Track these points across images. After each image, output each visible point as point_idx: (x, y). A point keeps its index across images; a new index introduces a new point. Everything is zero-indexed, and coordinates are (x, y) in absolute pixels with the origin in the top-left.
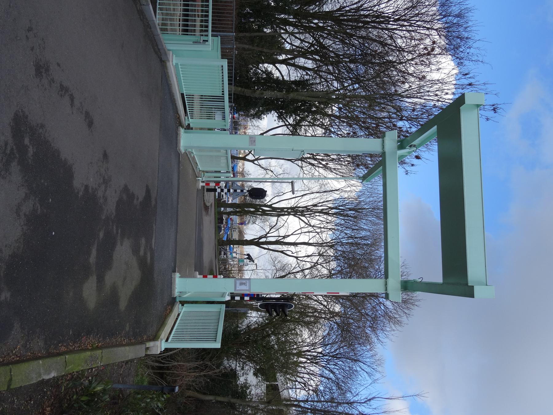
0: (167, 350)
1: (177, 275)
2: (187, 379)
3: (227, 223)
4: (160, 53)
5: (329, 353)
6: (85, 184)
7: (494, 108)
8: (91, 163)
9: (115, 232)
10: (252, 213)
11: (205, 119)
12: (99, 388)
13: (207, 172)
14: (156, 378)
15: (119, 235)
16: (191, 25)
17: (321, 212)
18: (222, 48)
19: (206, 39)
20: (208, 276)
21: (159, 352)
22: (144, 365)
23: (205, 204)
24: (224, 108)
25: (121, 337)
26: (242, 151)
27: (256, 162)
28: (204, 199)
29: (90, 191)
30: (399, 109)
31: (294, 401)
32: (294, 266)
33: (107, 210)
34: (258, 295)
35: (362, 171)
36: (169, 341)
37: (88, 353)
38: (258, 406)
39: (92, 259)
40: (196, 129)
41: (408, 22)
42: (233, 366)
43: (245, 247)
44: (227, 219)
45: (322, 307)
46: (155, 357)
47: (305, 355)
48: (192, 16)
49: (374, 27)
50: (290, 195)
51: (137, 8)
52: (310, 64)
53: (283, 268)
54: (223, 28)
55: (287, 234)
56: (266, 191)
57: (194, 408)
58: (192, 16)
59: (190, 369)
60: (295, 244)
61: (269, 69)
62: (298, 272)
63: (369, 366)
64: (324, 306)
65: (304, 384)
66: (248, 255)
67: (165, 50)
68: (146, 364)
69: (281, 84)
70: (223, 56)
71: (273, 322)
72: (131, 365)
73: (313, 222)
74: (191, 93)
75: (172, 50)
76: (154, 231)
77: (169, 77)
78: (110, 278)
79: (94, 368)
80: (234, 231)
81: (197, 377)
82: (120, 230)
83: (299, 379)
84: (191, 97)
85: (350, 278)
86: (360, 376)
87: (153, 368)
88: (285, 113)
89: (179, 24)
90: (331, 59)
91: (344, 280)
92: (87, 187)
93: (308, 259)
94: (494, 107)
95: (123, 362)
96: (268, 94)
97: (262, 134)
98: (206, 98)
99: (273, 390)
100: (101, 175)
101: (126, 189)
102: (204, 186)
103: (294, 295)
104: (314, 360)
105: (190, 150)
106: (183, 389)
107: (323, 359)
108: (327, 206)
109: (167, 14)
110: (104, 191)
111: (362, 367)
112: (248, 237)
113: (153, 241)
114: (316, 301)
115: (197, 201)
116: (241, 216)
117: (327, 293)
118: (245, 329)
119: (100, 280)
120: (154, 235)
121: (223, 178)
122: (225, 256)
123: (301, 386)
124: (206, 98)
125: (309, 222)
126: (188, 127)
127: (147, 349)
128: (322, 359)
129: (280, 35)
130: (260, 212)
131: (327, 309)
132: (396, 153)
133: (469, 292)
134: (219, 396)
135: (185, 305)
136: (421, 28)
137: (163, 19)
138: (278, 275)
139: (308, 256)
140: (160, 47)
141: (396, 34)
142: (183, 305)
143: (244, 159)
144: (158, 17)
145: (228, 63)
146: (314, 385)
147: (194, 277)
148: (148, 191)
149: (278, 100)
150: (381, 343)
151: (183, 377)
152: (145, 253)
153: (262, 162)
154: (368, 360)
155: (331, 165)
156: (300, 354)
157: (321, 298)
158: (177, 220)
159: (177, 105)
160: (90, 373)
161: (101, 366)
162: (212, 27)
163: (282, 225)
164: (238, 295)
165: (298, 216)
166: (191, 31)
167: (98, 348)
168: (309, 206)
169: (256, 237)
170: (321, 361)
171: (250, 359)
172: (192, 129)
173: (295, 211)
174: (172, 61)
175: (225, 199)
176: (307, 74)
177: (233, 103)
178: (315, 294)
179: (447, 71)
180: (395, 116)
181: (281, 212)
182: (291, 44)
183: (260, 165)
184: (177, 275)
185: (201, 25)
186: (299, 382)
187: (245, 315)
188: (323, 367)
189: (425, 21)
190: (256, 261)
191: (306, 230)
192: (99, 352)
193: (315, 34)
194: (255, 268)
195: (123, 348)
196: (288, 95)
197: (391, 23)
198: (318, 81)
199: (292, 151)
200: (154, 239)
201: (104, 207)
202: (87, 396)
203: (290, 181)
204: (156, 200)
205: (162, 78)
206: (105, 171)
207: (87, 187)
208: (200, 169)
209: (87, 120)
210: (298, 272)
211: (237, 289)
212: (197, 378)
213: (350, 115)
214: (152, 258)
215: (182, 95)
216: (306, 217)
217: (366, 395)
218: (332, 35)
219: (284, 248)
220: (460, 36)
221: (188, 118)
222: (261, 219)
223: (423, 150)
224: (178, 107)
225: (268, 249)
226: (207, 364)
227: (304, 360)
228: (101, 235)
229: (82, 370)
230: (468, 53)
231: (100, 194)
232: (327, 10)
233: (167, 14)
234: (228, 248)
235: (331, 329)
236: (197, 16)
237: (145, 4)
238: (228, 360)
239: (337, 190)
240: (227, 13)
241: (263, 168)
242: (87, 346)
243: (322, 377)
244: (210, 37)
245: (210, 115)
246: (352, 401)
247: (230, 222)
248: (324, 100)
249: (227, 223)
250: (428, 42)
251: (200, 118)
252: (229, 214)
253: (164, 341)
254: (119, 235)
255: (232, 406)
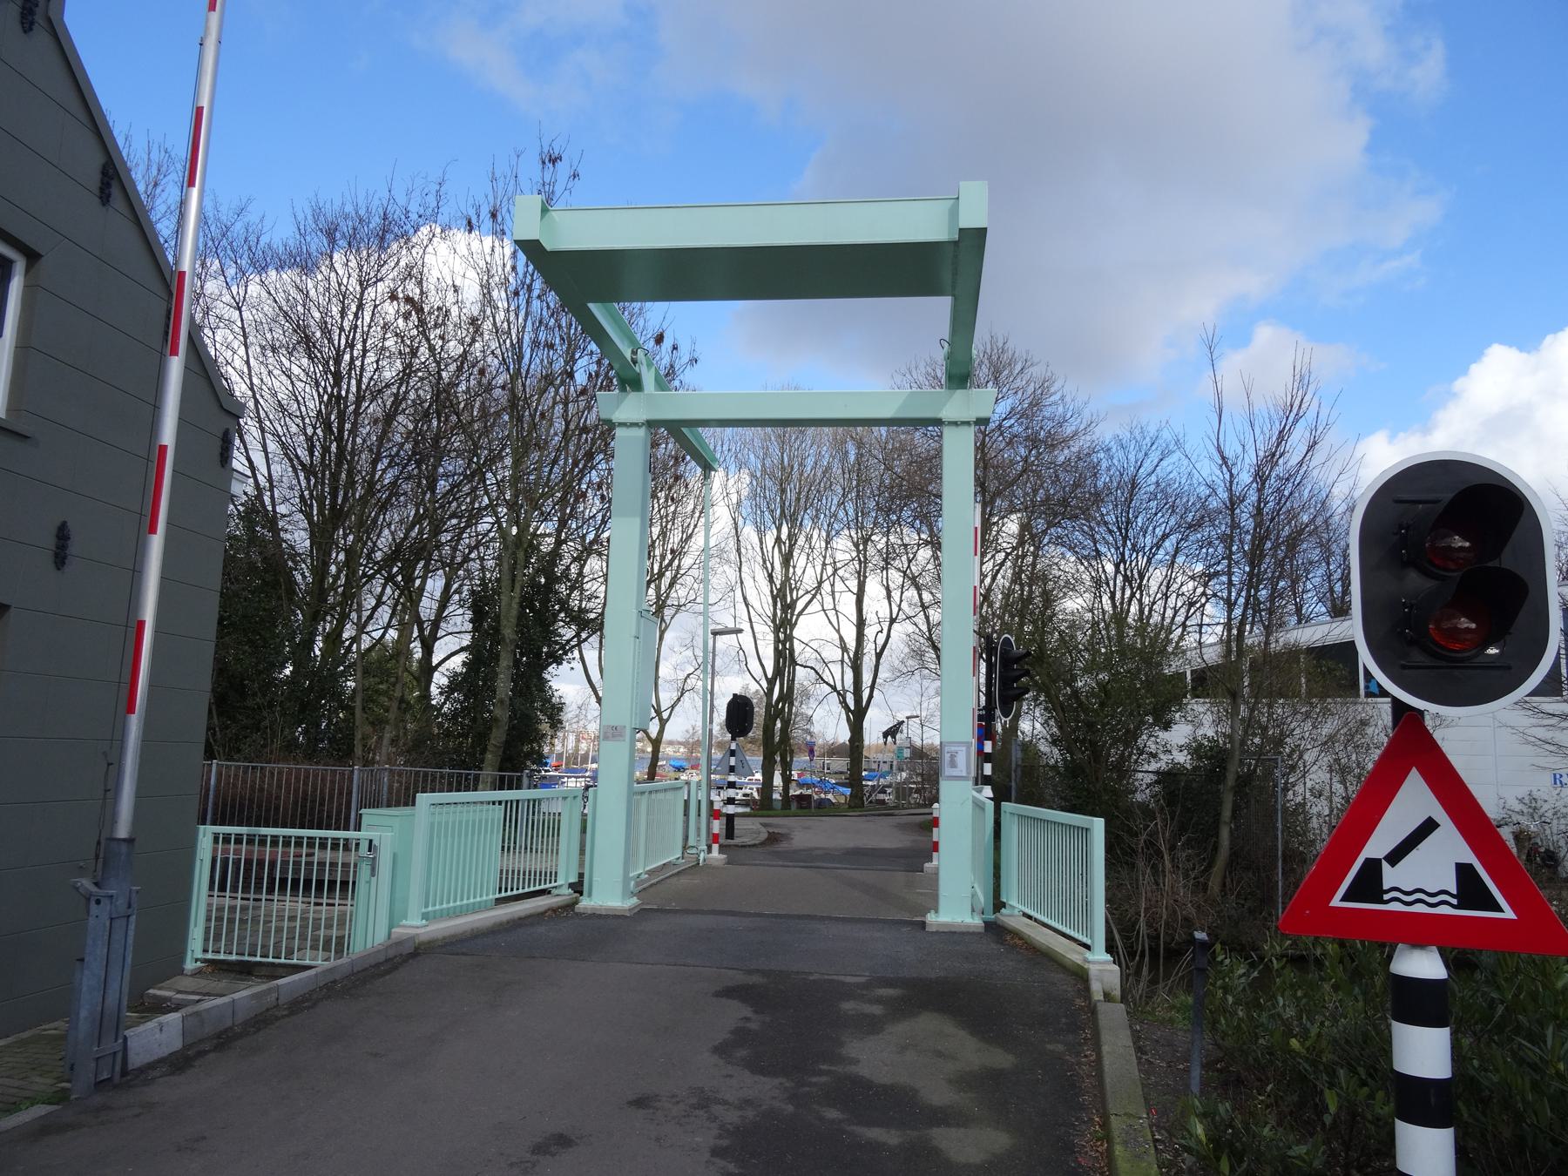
0: (1110, 948)
1: (931, 918)
2: (1182, 891)
3: (808, 786)
4: (396, 957)
5: (1117, 548)
6: (707, 1155)
7: (550, 161)
8: (658, 1139)
9: (824, 1079)
10: (786, 724)
11: (558, 842)
12: (1200, 1130)
13: (686, 838)
14: (1177, 973)
15: (833, 1068)
16: (330, 874)
17: (787, 559)
18: (389, 806)
19: (367, 843)
20: (935, 839)
21: (1116, 968)
22: (1147, 1003)
23: (763, 844)
24: (534, 801)
25: (1079, 1064)
26: (639, 745)
27: (665, 715)
28: (749, 846)
29: (725, 1143)
30: (548, 380)
31: (1229, 631)
32: (911, 628)
33: (774, 1098)
34: (980, 718)
35: (693, 472)
36: (1089, 942)
37: (1118, 1150)
38: (1243, 719)
39: (890, 1137)
40: (582, 864)
41: (344, 352)
42: (1149, 778)
43: (866, 742)
44: (801, 785)
45: (1009, 564)
46: (1128, 975)
47: (1122, 603)
48: (309, 871)
49: (354, 431)
50: (746, 639)
51: (283, 1017)
52: (435, 585)
53: (918, 654)
54: (341, 793)
55: (837, 642)
56: (735, 695)
57: (1251, 875)
58: (309, 871)
59: (1157, 884)
60: (861, 624)
61: (445, 681)
62: (927, 618)
63: (1146, 454)
64: (1006, 558)
65: (1191, 604)
66: (886, 735)
67: (388, 948)
68: (1144, 998)
69: (480, 657)
70: (410, 801)
71: (1043, 683)
72: (1146, 1039)
73: (809, 581)
74: (493, 881)
75: (391, 927)
76: (826, 977)
77: (454, 936)
78: (938, 1094)
79: (1153, 1135)
80: (828, 769)
81: (1176, 867)
82: (822, 1067)
83: (1180, 619)
84: (505, 878)
85: (939, 496)
86: (1171, 476)
87: (1153, 982)
88: (549, 647)
89: (328, 905)
90: (425, 536)
91: (945, 512)
92: (716, 1152)
93: (896, 595)
94: (547, 161)
95: (1139, 1059)
96: (504, 686)
97: (599, 700)
98: (509, 839)
99: (1205, 682)
100: (688, 1116)
101: (722, 1050)
102: (721, 846)
103: (979, 633)
104: (1135, 581)
105: (633, 883)
106: (1205, 901)
107: (1131, 561)
108: (774, 547)
109: (303, 937)
110: (727, 1107)
111: (1149, 470)
112: (844, 735)
113: (849, 979)
114: (994, 578)
115: (756, 865)
116: (792, 752)
117: (976, 554)
118: (1060, 750)
119: (942, 1117)
120: (835, 977)
121: (702, 795)
122: (889, 790)
123: (1198, 614)
124: (509, 839)
125: (807, 592)
126: (578, 888)
127: (1108, 997)
128: (1130, 564)
129: (363, 655)
130: (783, 707)
131: (1013, 551)
132: (650, 395)
133: (975, 239)
134: (1219, 814)
135: (1004, 899)
136: (359, 323)
137: (314, 947)
138: (933, 666)
139: (889, 596)
140: (382, 958)
141: (369, 383)
142: (1004, 905)
143: (656, 743)
144: (307, 962)
145: (424, 791)
146: (1191, 584)
147: (936, 873)
148: (729, 992)
149: (517, 663)
150: (1094, 425)
151: (1176, 901)
152: (879, 1001)
153: (667, 698)
154: (1132, 458)
155: (675, 539)
156: (1119, 617)
157: (988, 567)
158: (799, 917)
159: (522, 914)
160: (1166, 1147)
161: (1148, 1118)
162: (338, 829)
163: (815, 654)
164: (980, 768)
165: (795, 617)
166: (346, 873)
167: (1105, 1125)
168: (772, 591)
169: (844, 716)
170: (1137, 565)
171: (1131, 737)
172: (581, 875)
173: (784, 625)
174: (418, 927)
175: (752, 789)
176: (458, 591)
177: (522, 772)
178: (977, 583)
179: (459, 266)
180: (561, 390)
181: (785, 657)
182: (386, 629)
183: (673, 707)
184: (931, 918)
185: (332, 849)
186: (1187, 618)
187: (1028, 747)
188: (1149, 561)
189: (343, 313)
190: (901, 717)
191: (828, 603)
192: (1116, 1124)
193: (363, 571)
194: (917, 720)
195: (1107, 1061)
196: (508, 641)
197: (343, 393)
198: (476, 565)
199: (641, 639)
200: (842, 978)
201: (764, 1107)
202: (1218, 1159)
203: (711, 636)
204: (750, 972)
205: (457, 954)
206: (678, 1102)
207: (716, 1152)
208: (679, 855)
209: (552, 1149)
210: (927, 618)
211: (964, 774)
212: (1178, 867)
213: (559, 495)
214: (889, 983)
215: (499, 901)
216: (798, 599)
217: (1213, 467)
218: (366, 529)
219: (869, 649)
220: (381, 233)
221: (556, 887)
222: (801, 703)
223: (641, 323)
224: (528, 912)
225: (872, 687)
226: (1145, 842)
227: (1134, 608)
228: (832, 1114)
229: (1159, 1167)
230: (420, 216)
231: (732, 1117)
232: (308, 543)
233: (303, 937)
234: (870, 783)
235: (1058, 542)
236: (310, 859)
237: (274, 995)
238: (1134, 792)
239: (736, 524)
240: (306, 784)
241: (679, 700)
242: (1102, 1153)
243: (1173, 563)
244: (363, 834)
245: (549, 828)
246: (1225, 496)
247: (808, 777)
248: (521, 555)
249: (808, 786)
250: (390, 309)
251: (557, 853)
252: (787, 780)
253: (1089, 955)
254: (833, 1068)
255: (1244, 781)
